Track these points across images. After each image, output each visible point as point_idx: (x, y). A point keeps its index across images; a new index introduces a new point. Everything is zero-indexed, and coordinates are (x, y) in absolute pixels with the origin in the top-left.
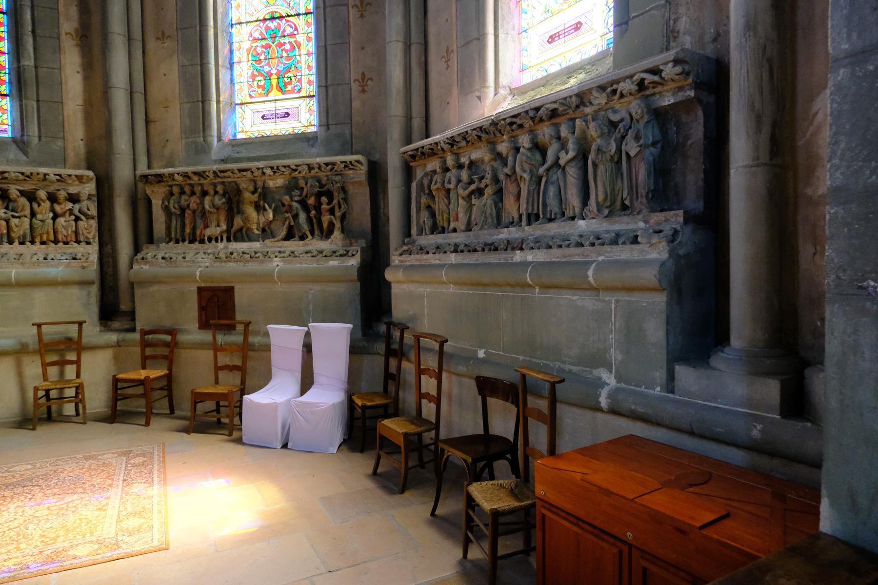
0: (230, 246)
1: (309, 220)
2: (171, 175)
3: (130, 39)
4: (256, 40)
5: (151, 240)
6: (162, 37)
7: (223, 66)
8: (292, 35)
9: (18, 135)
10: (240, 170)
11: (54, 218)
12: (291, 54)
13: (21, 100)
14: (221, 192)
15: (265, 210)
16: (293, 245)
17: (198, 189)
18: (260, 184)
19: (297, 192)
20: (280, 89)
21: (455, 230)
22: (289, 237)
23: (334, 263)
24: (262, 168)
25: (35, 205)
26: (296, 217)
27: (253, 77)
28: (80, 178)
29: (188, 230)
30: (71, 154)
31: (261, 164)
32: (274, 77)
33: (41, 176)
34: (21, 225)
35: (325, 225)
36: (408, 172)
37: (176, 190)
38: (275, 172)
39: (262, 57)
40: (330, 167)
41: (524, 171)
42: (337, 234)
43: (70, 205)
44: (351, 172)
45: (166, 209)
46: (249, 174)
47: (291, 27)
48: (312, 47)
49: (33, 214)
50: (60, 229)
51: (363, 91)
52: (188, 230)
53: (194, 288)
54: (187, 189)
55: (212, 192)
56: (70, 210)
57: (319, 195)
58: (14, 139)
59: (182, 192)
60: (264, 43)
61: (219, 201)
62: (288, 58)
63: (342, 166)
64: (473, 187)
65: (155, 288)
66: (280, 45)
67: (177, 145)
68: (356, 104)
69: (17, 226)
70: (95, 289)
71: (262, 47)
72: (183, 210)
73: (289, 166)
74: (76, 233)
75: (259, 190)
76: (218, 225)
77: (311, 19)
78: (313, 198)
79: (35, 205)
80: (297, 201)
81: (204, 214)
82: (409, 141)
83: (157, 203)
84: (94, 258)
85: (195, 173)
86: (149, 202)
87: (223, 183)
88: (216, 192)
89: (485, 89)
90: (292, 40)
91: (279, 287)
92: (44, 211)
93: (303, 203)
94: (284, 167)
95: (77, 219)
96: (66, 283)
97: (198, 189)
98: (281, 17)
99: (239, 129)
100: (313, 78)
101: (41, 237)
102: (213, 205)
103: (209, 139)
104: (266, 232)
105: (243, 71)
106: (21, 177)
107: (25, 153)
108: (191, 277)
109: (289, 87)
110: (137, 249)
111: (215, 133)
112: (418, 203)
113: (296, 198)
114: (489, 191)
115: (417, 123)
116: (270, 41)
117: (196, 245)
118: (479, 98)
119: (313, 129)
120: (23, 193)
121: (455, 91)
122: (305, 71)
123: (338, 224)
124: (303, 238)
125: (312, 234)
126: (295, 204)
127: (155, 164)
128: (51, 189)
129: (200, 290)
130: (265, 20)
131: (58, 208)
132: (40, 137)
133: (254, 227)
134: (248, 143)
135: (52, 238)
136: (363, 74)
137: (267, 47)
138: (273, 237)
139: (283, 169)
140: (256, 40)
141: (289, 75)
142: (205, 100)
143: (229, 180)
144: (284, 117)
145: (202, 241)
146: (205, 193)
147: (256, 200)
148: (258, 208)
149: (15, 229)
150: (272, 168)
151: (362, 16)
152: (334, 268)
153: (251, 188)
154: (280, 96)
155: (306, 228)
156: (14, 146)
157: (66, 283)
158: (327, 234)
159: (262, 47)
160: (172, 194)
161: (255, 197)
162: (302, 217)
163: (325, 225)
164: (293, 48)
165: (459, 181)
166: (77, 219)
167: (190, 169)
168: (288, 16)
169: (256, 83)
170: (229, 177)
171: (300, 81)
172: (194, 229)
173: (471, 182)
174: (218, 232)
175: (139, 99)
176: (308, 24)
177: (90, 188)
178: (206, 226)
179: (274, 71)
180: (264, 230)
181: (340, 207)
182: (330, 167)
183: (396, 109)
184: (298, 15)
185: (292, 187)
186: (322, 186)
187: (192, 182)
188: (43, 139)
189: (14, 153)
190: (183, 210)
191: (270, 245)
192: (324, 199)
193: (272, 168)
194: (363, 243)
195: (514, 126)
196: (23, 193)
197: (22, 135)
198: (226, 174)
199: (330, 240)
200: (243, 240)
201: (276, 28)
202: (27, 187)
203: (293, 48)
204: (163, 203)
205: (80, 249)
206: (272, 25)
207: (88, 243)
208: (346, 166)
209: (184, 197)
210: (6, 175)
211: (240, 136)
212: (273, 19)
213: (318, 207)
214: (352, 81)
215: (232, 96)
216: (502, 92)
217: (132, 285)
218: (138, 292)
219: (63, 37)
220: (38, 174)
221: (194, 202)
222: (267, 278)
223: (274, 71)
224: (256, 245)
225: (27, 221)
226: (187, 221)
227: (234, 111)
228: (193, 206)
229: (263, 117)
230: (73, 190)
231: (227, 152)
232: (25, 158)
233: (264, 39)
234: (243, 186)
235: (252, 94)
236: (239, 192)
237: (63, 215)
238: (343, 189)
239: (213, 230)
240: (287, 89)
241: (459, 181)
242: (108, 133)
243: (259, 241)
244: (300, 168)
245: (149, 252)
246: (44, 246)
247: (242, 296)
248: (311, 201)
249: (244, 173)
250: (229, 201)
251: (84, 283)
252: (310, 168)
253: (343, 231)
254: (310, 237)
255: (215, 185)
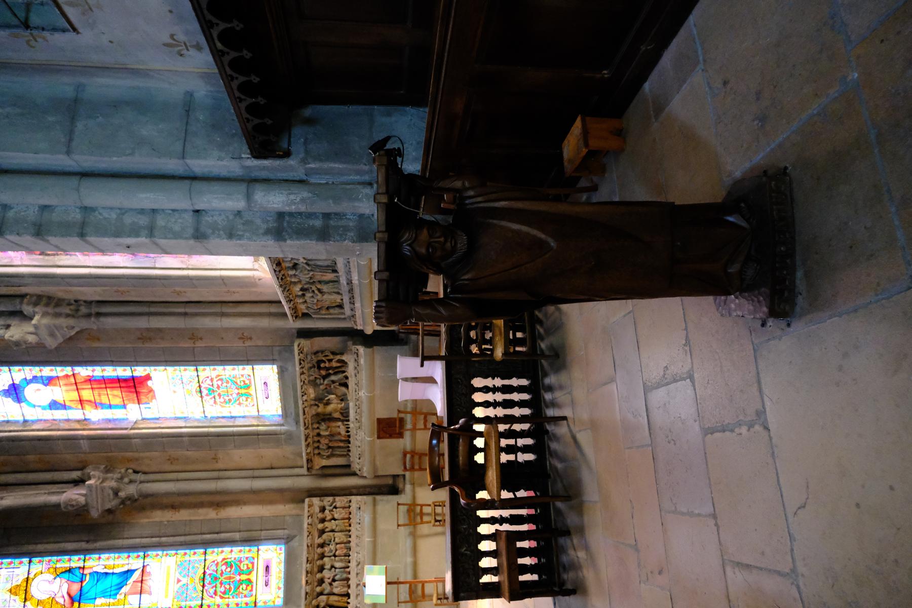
0: (352, 420)
1: (335, 373)
2: (307, 454)
3: (218, 478)
4: (215, 402)
5: (349, 466)
6: (215, 459)
7: (234, 422)
8: (212, 380)
9: (283, 541)
10: (304, 414)
11: (335, 520)
12: (225, 381)
13: (261, 540)
14: (318, 425)
15: (329, 400)
16: (351, 383)
17: (316, 439)
18: (313, 402)
19: (318, 381)
20: (249, 387)
21: (342, 300)
22: (346, 385)
23: (362, 361)
24: (303, 401)
25: (327, 530)
26: (333, 382)
27: (240, 404)
28: (310, 506)
29: (342, 444)
30: (294, 512)
31: (300, 402)
32: (240, 391)
33: (309, 526)
34: (340, 537)
35: (339, 365)
36: (306, 315)
37: (316, 451)
38: (305, 394)
39: (227, 398)
40: (302, 362)
41: (309, 273)
42: (344, 358)
43: (327, 512)
44: (305, 349)
45: (328, 457)
46: (306, 410)
47: (206, 381)
48: (219, 368)
49: (333, 531)
50: (341, 516)
51: (251, 338)
52: (342, 444)
53: (378, 441)
54: (316, 445)
55: (317, 431)
56: (330, 511)
57: (319, 368)
58: (286, 544)
59: (318, 448)
60: (217, 397)
61: (323, 426)
62: (227, 382)
63: (301, 355)
64: (316, 292)
65: (378, 463)
66: (218, 387)
67: (287, 450)
68: (260, 343)
69: (340, 539)
70: (378, 497)
71: (220, 398)
72: (329, 447)
73: (302, 386)
74: (344, 508)
75: (317, 403)
76: (339, 427)
77: (200, 368)
78: (322, 371)
79: (327, 530)
80: (324, 381)
81: (332, 435)
82: (285, 315)
83: (325, 462)
84: (359, 498)
85: (306, 440)
86: (324, 467)
87: (312, 424)
88: (318, 428)
89: (255, 277)
90: (215, 380)
91: (378, 392)
92: (330, 525)
93: (324, 378)
94: (302, 388)
95: (335, 507)
96: (374, 512)
97: (316, 439)
98: (200, 386)
99: (275, 413)
100: (241, 367)
101: (347, 526)
102: (326, 430)
103: (283, 431)
104: (343, 399)
105: (236, 410)
106: (310, 537)
107: (295, 536)
108: (372, 444)
109: (247, 382)
110: (354, 474)
111: (278, 428)
112: (325, 314)
113: (322, 381)
114: (319, 286)
115: (273, 309)
116: (216, 394)
117: (351, 439)
118: (260, 280)
119: (275, 367)
120: (320, 536)
121: (254, 290)
122: (233, 373)
123: (338, 357)
124: (347, 378)
125: (344, 372)
126: (326, 382)
127: (299, 464)
128: (317, 521)
129: (379, 437)
130: (202, 397)
131: (329, 518)
132: (284, 529)
133: (340, 406)
134: (284, 408)
135: (347, 521)
136: (240, 338)
137: (219, 395)
138: (346, 394)
139: (303, 389)
140: (215, 402)
141: (239, 382)
142: (257, 434)
143: (310, 420)
144: (267, 385)
145: (349, 436)
146: (319, 435)
147: (322, 405)
148: (328, 403)
149: (342, 540)
150: (303, 396)
151: (201, 339)
152: (365, 362)
153: (316, 407)
154: (254, 573)
155: (341, 376)
156: (291, 544)
157: (374, 512)
158: (344, 363)
159: (220, 398)
160: (319, 454)
161: (321, 406)
162: (333, 378)
163: (339, 365)
164: (226, 564)
165: (313, 297)
166: (335, 507)
167: (303, 443)
168: (199, 382)
169: (244, 592)
170: (308, 421)
171: (242, 376)
172: (341, 441)
173: (313, 291)
174: (343, 427)
175: (257, 473)
176: (204, 370)
177: (316, 501)
178: (339, 434)
179: (236, 391)
180: (342, 400)
181: (327, 356)
182: (302, 362)
183: (265, 323)
184: (198, 376)
185: (314, 383)
186: (314, 367)
187: (311, 442)
188: (285, 527)
189: (295, 543)
190: (329, 447)
191: (351, 395)
192: (322, 365)
193: (303, 396)
194: (350, 343)
195: (283, 277)
196: (320, 536)
197: (283, 539)
198: (306, 422)
199: (348, 363)
200: (348, 412)
201: (207, 390)
202: (316, 534)
203: (226, 564)
204: (324, 459)
205: (354, 506)
206: (205, 392)
207: (350, 501)
208: (302, 353)
209: (321, 447)
210: (309, 545)
211: (280, 412)
212: (201, 392)
213: (327, 369)
214: (244, 345)
215: (253, 417)
216: (256, 266)
217: (377, 477)
218: (380, 473)
219: (220, 516)
220: (308, 528)
221: (324, 441)
222: (371, 400)
223: (236, 391)
224: (351, 405)
225: (336, 534)
226: (336, 445)
227: (262, 416)
228: (327, 441)
229: (267, 398)
230: (317, 510)
231: (291, 420)
232: (297, 537)
233: (214, 397)
234: (314, 412)
235: (252, 404)
236: (318, 415)
237: (333, 515)
238: (316, 353)
239: (342, 430)
240: (249, 384)
241: (313, 297)
242: (281, 491)
243: (349, 403)
244: (303, 380)
245: (355, 467)
246: (352, 525)
247: (383, 414)
248: (323, 373)
249: (306, 412)
250: (324, 420)
251: (375, 503)
252: (302, 373)
253: (342, 354)
254: (346, 373)
255: (313, 429)
